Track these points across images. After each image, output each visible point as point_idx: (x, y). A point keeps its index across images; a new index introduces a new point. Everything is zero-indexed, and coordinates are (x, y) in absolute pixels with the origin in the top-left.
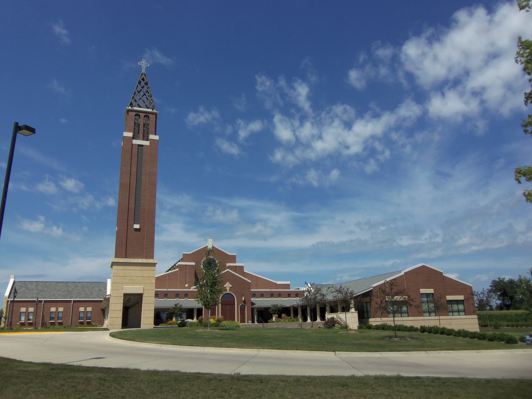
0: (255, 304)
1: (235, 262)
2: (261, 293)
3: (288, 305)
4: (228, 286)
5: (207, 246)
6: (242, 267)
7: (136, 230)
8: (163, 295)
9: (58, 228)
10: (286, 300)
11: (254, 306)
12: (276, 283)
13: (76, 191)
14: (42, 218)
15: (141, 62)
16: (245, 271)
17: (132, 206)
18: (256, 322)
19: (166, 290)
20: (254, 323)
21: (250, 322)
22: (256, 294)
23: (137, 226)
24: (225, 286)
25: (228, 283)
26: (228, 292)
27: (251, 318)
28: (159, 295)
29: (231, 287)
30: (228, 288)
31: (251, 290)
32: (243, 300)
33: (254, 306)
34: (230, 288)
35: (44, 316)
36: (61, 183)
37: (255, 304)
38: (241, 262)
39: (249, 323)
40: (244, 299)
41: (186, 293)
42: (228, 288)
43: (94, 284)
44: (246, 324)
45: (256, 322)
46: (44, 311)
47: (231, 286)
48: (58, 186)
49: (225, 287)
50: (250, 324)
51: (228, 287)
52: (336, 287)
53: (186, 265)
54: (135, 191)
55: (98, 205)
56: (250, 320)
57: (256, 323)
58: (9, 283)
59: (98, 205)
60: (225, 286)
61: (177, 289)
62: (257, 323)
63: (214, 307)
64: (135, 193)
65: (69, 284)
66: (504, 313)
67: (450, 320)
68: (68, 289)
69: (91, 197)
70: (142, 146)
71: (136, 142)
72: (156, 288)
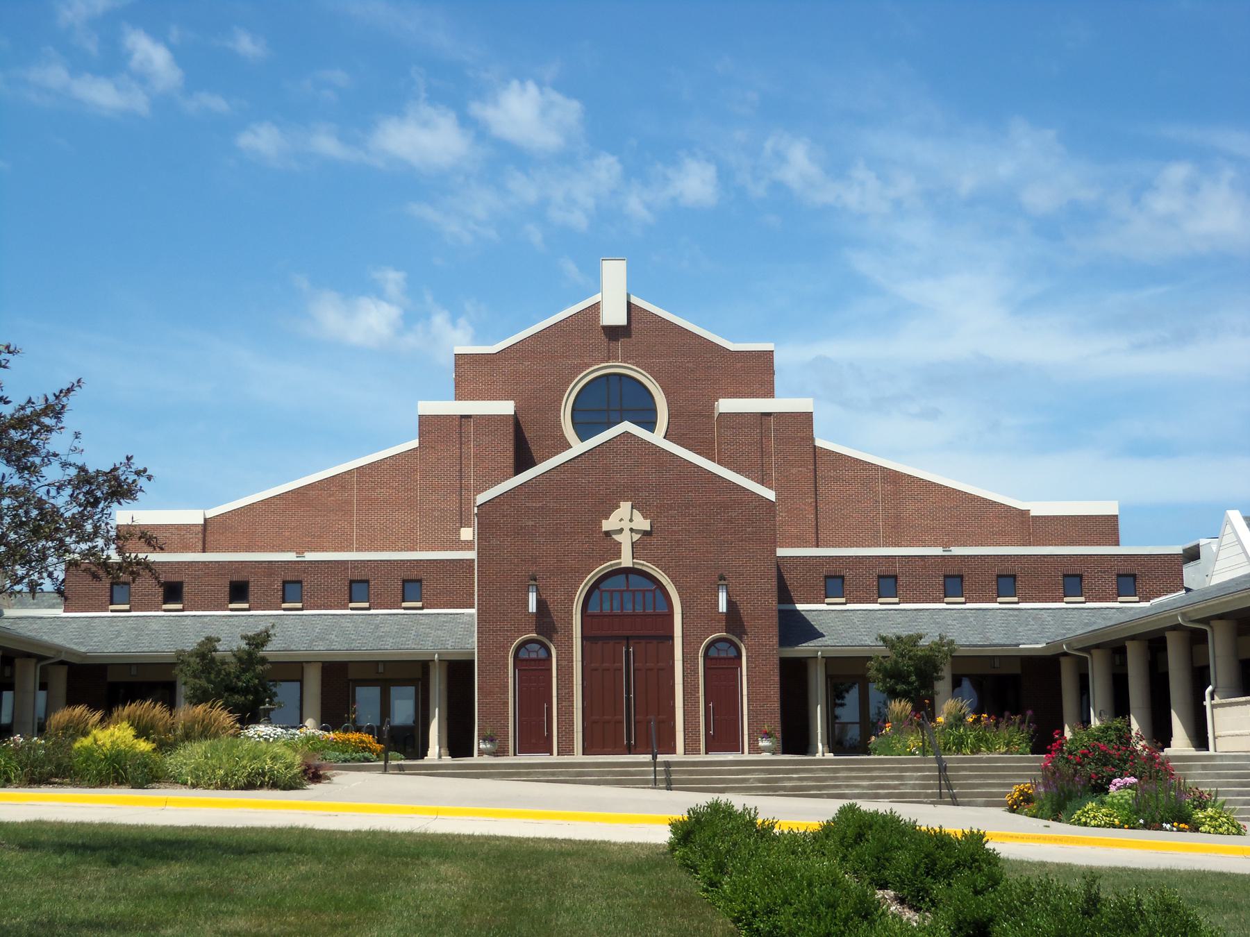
0: (822, 635)
1: (769, 393)
2: (883, 570)
3: (1033, 644)
4: (626, 525)
5: (596, 307)
6: (805, 420)
8: (278, 585)
9: (453, 322)
10: (1045, 614)
11: (804, 649)
12: (1024, 513)
13: (547, 139)
14: (393, 279)
16: (819, 443)
18: (820, 745)
19: (291, 556)
20: (805, 752)
21: (764, 743)
22: (847, 574)
24: (607, 525)
25: (625, 506)
26: (626, 560)
27: (775, 723)
28: (305, 584)
29: (645, 533)
30: (625, 540)
31: (781, 552)
32: (723, 607)
33: (804, 649)
34: (636, 537)
36: (476, 109)
37: (822, 635)
38: (800, 393)
39: (759, 750)
40: (730, 603)
41: (413, 575)
42: (625, 540)
44: (747, 756)
45: (820, 745)
47: (645, 525)
48: (466, 121)
49: (608, 534)
50: (766, 756)
51: (627, 532)
53: (462, 417)
55: (635, 204)
56: (767, 735)
57: (821, 752)
58: (1168, 673)
59: (635, 204)
60: (607, 525)
62: (830, 756)
63: (542, 654)
67: (1217, 659)
69: (607, 168)
72: (780, 603)
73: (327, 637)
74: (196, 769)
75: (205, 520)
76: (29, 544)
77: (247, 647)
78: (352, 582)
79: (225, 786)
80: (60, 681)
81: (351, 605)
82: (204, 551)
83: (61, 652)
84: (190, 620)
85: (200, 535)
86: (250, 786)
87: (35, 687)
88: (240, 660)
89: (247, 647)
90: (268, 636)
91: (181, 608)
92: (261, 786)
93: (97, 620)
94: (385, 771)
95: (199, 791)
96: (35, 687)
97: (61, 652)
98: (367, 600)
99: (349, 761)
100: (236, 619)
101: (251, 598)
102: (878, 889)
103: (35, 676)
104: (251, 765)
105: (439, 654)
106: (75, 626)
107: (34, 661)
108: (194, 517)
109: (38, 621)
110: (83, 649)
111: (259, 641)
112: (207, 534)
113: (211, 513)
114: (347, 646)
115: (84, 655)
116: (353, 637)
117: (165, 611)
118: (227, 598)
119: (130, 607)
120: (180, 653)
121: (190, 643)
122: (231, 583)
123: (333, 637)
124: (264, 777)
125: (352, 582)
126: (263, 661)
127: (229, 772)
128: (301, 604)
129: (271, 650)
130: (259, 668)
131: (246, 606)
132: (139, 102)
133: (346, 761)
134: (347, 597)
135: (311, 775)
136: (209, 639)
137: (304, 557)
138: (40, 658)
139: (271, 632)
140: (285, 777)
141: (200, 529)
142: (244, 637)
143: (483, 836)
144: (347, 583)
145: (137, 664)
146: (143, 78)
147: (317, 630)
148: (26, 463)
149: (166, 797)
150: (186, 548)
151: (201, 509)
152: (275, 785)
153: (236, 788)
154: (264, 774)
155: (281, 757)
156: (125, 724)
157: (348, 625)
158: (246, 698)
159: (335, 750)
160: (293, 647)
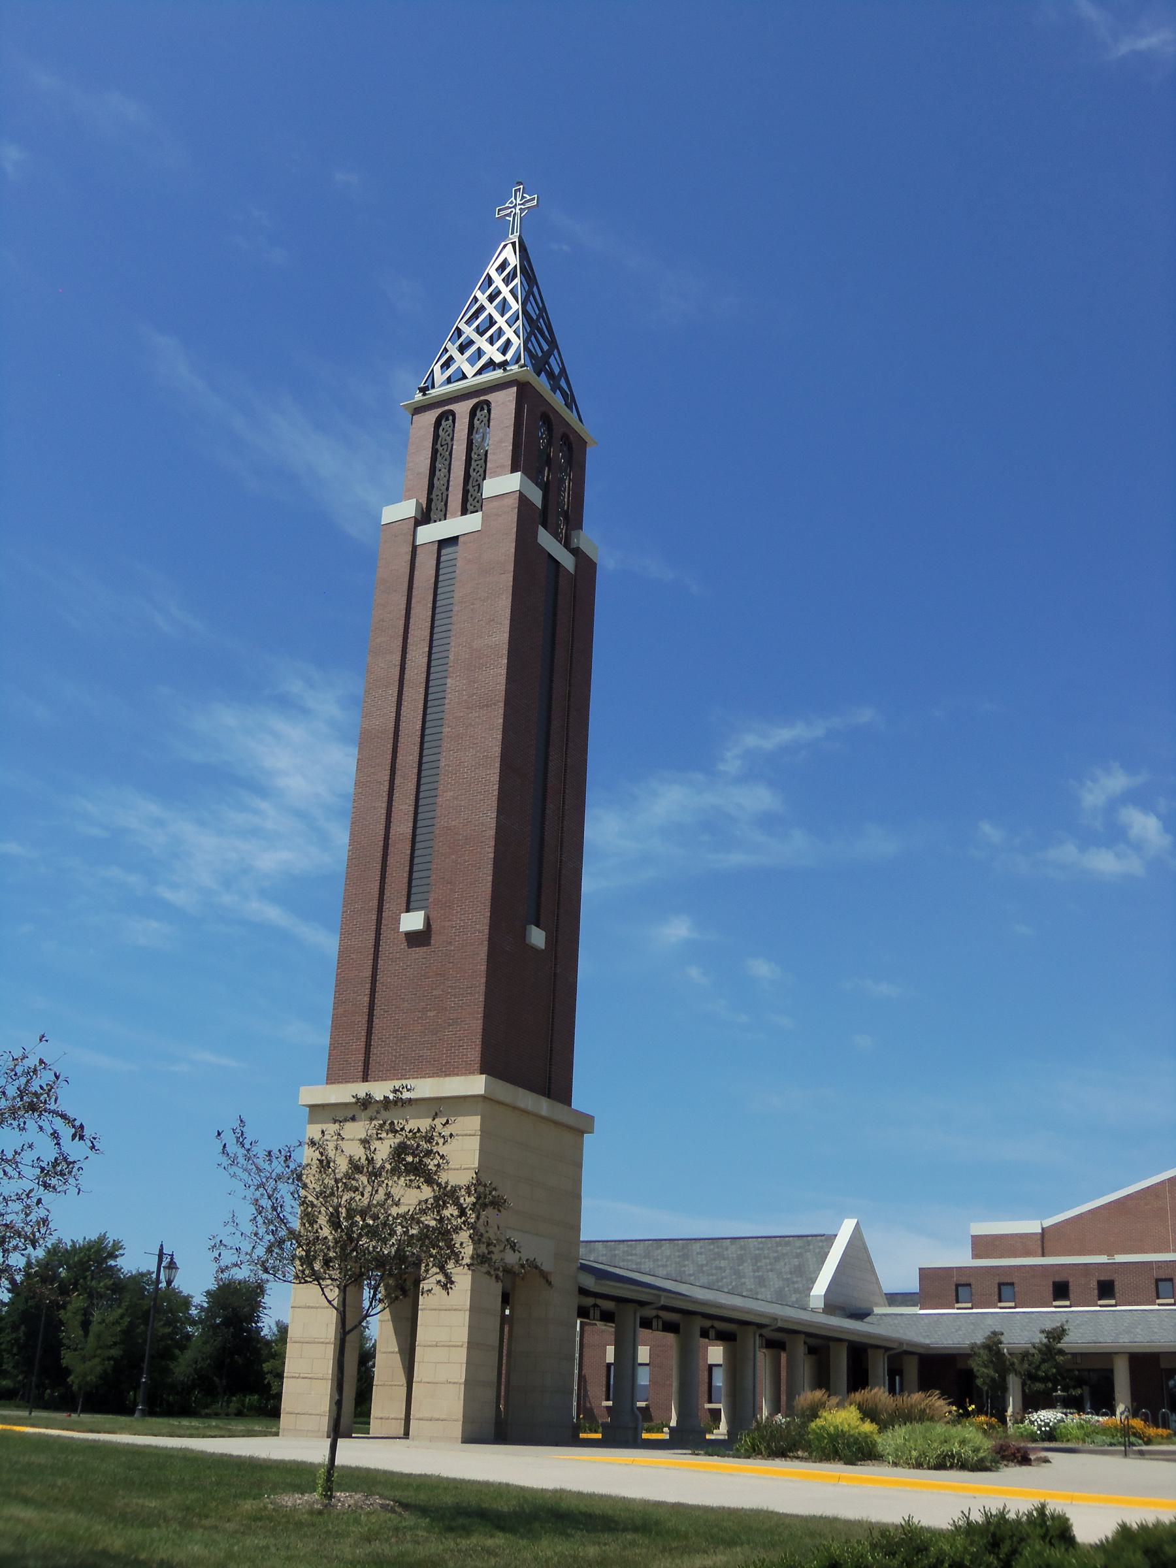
7: (416, 939)
15: (507, 205)
17: (402, 828)
23: (412, 921)
28: (973, 1287)
35: (585, 1382)
41: (963, 1280)
43: (788, 1244)
46: (585, 1359)
52: (47, 1041)
54: (416, 754)
61: (1167, 1250)
64: (416, 765)
65: (697, 1247)
66: (57, 1434)
68: (683, 1269)
70: (453, 541)
71: (429, 533)
73: (1133, 1330)
74: (897, 1450)
75: (1043, 1229)
76: (373, 1266)
77: (1045, 1340)
78: (1158, 1281)
79: (919, 1466)
80: (912, 1370)
81: (1158, 1301)
82: (1043, 1255)
83: (903, 1344)
84: (1036, 1316)
85: (1039, 1243)
86: (940, 1466)
87: (884, 1374)
88: (1040, 1350)
89: (1045, 1340)
90: (1064, 1330)
91: (1014, 1305)
92: (951, 1467)
93: (944, 1317)
94: (1126, 1455)
95: (898, 1470)
96: (884, 1374)
97: (903, 1344)
98: (1172, 1296)
99: (1115, 1445)
100: (1059, 1315)
101: (1071, 1296)
102: (728, 1562)
103: (884, 1364)
104: (941, 1448)
105: (1008, 1349)
106: (926, 1321)
107: (882, 1351)
108: (1033, 1227)
109: (899, 1317)
110: (927, 1341)
111: (1057, 1334)
112: (1045, 1241)
113: (1047, 1223)
114: (1148, 1339)
115: (927, 1347)
116: (1156, 1330)
117: (1001, 1308)
118: (1052, 1299)
119: (1116, 1302)
120: (973, 1346)
121: (979, 1338)
122: (1054, 1283)
123: (1138, 1330)
124: (954, 1460)
125: (1158, 1281)
126: (1061, 1352)
127: (922, 1453)
128: (1114, 1301)
129: (1067, 1343)
130: (1060, 1359)
131: (1068, 1303)
132: (1134, 866)
133: (1111, 1444)
134: (1154, 1294)
135: (1020, 1458)
136: (995, 1333)
137: (1114, 1259)
138: (887, 1349)
139: (1066, 1327)
140: (973, 1460)
141: (1039, 1237)
142: (1042, 1332)
143: (752, 1510)
144: (1153, 1281)
145: (1082, 1354)
146: (1138, 847)
147: (1125, 1324)
148: (448, 1203)
149: (839, 1473)
150: (1028, 1253)
151: (1037, 1219)
152: (964, 1466)
153: (929, 1468)
154: (952, 1457)
155: (969, 1442)
156: (853, 1408)
157: (1154, 1319)
158: (1046, 1386)
159: (1104, 1434)
160: (1101, 1340)
